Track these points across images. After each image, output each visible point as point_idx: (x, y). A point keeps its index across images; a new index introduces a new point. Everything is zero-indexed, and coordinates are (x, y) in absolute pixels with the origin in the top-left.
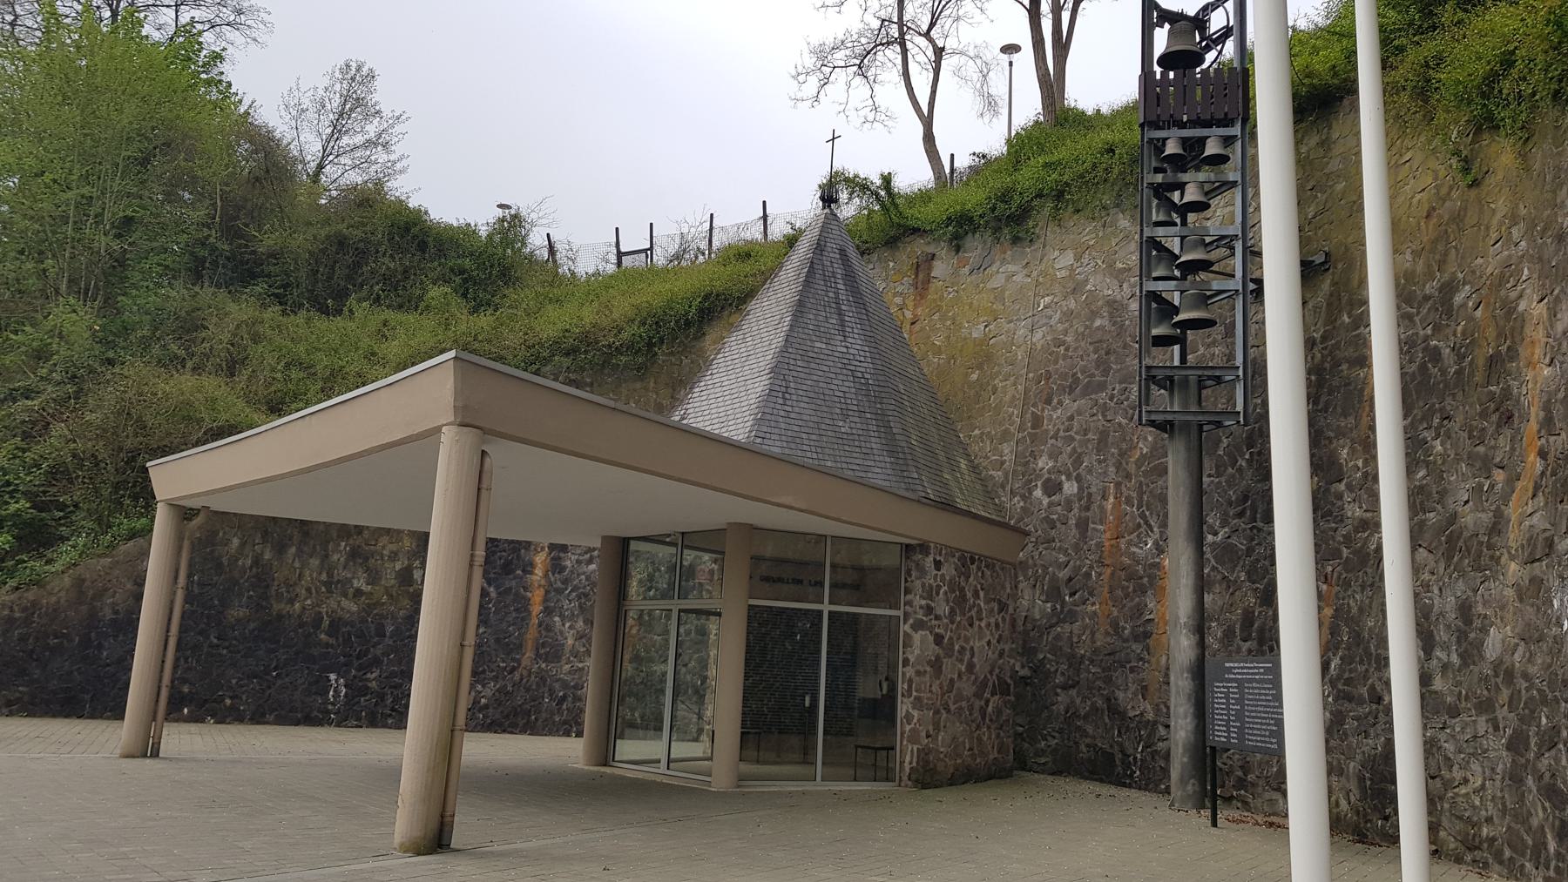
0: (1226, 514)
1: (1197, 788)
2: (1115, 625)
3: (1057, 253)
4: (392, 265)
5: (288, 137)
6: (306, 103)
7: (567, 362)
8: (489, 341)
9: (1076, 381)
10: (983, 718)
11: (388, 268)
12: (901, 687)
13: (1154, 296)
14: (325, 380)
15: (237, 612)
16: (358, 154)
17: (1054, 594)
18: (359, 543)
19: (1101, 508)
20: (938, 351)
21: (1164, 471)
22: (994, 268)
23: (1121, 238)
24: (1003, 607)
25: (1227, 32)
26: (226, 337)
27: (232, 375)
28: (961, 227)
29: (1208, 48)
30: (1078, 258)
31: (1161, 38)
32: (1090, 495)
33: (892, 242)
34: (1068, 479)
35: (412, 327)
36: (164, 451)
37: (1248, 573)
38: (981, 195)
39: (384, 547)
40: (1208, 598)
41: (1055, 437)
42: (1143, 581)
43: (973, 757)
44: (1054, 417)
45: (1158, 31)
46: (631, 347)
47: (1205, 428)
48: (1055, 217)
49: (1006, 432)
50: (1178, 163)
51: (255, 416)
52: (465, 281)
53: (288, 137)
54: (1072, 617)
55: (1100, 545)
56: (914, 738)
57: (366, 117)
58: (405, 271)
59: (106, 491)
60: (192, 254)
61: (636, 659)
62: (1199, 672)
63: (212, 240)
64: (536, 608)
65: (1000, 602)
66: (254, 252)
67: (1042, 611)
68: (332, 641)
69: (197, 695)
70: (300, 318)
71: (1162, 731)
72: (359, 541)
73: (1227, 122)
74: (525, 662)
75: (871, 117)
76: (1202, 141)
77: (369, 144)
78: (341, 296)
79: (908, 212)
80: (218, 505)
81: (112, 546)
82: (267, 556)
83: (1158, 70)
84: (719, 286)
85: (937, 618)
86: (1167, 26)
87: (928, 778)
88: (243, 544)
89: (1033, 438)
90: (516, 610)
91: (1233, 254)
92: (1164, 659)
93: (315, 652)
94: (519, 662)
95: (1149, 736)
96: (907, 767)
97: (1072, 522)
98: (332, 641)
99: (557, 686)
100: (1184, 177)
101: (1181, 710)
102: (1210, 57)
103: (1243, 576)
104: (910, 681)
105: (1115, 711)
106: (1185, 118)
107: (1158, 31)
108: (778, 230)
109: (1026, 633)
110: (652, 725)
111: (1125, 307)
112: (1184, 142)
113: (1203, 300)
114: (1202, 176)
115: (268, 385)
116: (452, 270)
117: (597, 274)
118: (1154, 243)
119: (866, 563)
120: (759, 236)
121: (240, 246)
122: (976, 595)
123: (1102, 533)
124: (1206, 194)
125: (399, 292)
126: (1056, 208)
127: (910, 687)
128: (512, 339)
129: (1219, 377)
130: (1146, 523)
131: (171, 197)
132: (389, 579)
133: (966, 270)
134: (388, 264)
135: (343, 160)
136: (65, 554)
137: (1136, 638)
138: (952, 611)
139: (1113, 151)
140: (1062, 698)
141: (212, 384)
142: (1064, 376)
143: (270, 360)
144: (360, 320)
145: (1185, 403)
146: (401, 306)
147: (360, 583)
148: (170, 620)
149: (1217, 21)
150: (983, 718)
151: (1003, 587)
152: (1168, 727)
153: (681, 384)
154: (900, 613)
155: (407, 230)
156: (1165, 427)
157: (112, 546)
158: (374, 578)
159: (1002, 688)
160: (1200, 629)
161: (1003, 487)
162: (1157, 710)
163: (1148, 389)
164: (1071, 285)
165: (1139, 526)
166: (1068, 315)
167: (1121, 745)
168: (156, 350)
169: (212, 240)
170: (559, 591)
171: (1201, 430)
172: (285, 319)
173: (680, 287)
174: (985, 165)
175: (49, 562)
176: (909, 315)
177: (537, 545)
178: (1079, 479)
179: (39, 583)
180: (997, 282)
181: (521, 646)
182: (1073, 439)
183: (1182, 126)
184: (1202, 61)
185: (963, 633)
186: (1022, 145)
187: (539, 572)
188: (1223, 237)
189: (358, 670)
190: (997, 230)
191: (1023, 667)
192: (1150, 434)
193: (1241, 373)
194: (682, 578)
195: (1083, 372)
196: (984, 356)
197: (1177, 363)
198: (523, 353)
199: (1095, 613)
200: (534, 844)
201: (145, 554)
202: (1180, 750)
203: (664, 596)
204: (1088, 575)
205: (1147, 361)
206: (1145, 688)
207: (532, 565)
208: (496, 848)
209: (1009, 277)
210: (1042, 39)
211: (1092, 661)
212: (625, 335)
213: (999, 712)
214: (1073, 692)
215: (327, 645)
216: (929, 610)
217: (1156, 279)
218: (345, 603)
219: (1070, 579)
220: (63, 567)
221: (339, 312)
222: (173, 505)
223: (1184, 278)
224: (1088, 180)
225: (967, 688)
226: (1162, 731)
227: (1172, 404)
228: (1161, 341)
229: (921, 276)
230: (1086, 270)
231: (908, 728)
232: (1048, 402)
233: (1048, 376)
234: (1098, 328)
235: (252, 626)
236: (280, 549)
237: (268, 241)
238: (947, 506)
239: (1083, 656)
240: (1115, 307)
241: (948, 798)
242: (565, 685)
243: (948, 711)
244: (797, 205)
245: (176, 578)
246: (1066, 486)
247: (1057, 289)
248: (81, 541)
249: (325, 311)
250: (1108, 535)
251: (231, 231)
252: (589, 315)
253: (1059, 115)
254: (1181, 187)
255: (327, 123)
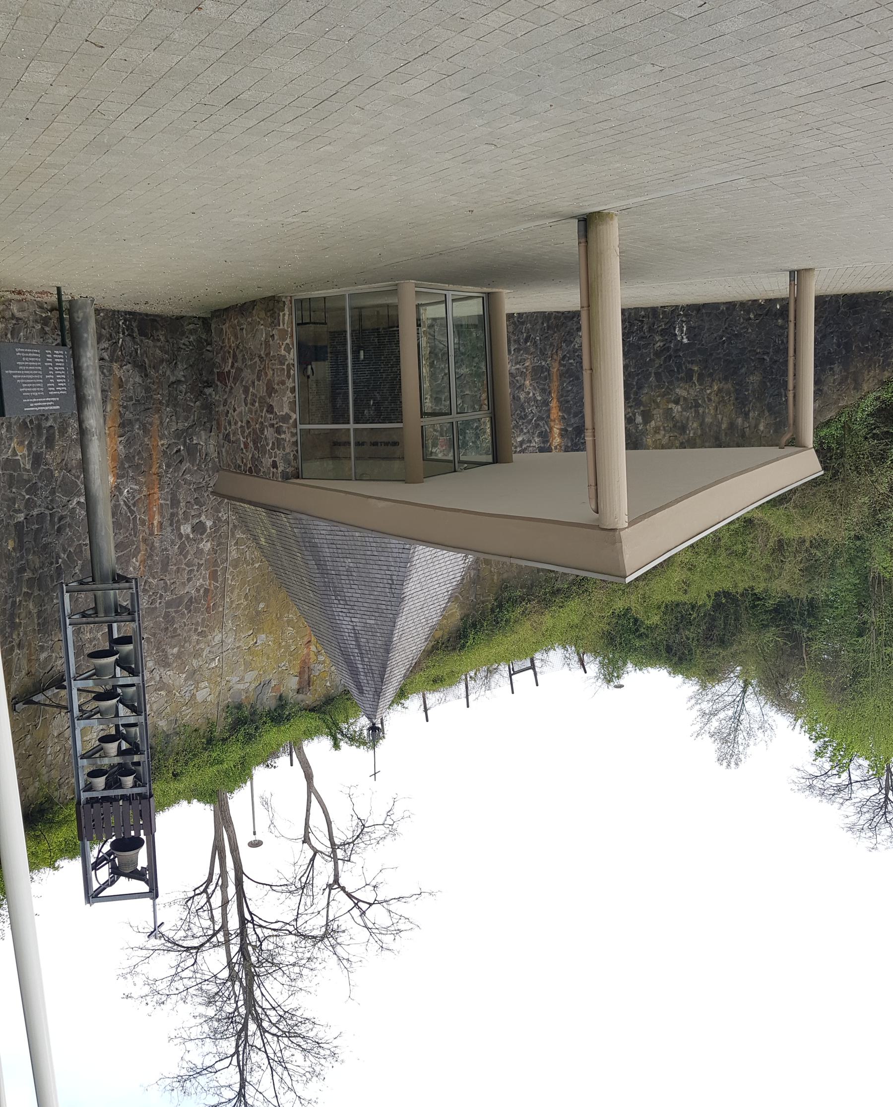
0: (72, 518)
1: (75, 315)
2: (146, 431)
3: (209, 699)
4: (687, 633)
5: (768, 706)
6: (759, 733)
7: (559, 585)
8: (614, 591)
9: (188, 608)
10: (234, 352)
11: (689, 630)
12: (294, 372)
13: (133, 673)
14: (719, 547)
15: (754, 379)
16: (721, 705)
17: (192, 450)
18: (683, 437)
19: (161, 514)
20: (289, 622)
21: (117, 546)
22: (253, 686)
23: (160, 712)
24: (227, 437)
25: (96, 866)
26: (787, 566)
27: (779, 541)
28: (280, 714)
29: (109, 854)
30: (193, 696)
31: (142, 861)
32: (171, 525)
33: (329, 700)
34: (188, 535)
35: (665, 591)
36: (815, 483)
37: (52, 476)
38: (266, 738)
39: (664, 436)
40: (79, 456)
41: (200, 565)
42: (127, 465)
43: (239, 324)
44: (201, 580)
45: (145, 865)
46: (514, 602)
47: (90, 579)
48: (212, 725)
49: (235, 566)
50: (124, 770)
51: (760, 515)
52: (637, 630)
53: (768, 706)
54: (178, 434)
55: (161, 489)
56: (283, 334)
57: (719, 732)
58: (677, 630)
59: (848, 451)
60: (816, 619)
61: (478, 375)
62: (81, 402)
63: (805, 630)
64: (554, 404)
65: (229, 441)
66: (778, 626)
67: (199, 437)
68: (689, 366)
69: (768, 319)
70: (741, 587)
71: (106, 356)
72: (682, 438)
73: (92, 801)
74: (556, 365)
75: (353, 790)
76: (108, 786)
77: (714, 714)
78: (717, 606)
79: (319, 723)
80: (774, 451)
81: (840, 414)
82: (740, 420)
83: (143, 836)
84: (455, 656)
85: (272, 425)
86: (139, 868)
87: (270, 305)
88: (756, 426)
89: (215, 564)
90: (568, 402)
91: (79, 706)
92: (108, 409)
93: (700, 357)
94: (560, 365)
95: (115, 351)
96: (287, 312)
97: (182, 504)
98: (689, 366)
99: (532, 350)
100: (117, 760)
101: (91, 372)
102: (107, 848)
103: (56, 474)
104: (289, 376)
105: (141, 367)
106: (121, 803)
107: (145, 865)
108: (414, 703)
109: (210, 420)
110: (461, 328)
111: (157, 663)
112: (120, 786)
113: (98, 673)
114: (106, 761)
115: (755, 537)
116: (647, 636)
117: (547, 651)
118: (136, 711)
119: (330, 462)
120: (428, 695)
121: (787, 629)
122: (246, 445)
123: (160, 497)
124: (102, 749)
125: (679, 615)
126: (211, 732)
127: (289, 372)
128: (598, 595)
129: (84, 617)
130: (129, 507)
131: (836, 654)
132: (657, 413)
133: (273, 683)
134: (690, 633)
135: (730, 699)
136: (869, 404)
137: (130, 422)
138: (262, 432)
139: (174, 775)
140: (180, 374)
141: (791, 533)
142: (197, 610)
143: (756, 555)
144: (701, 593)
145: (106, 597)
146: (677, 605)
147: (676, 409)
148: (795, 369)
149: (104, 874)
150: (234, 352)
151: (227, 452)
152: (102, 359)
153: (472, 582)
154: (300, 427)
155: (680, 659)
156: (118, 578)
157: (840, 414)
158: (668, 413)
159: (223, 377)
160: (82, 432)
161: (235, 526)
162: (110, 370)
163: (133, 605)
164: (197, 676)
165: (134, 505)
166: (197, 654)
167: (135, 343)
168: (830, 550)
169: (805, 630)
170: (541, 418)
171: (93, 580)
172: (751, 584)
173: (484, 652)
174: (267, 758)
175: (878, 398)
176: (313, 648)
177: (560, 450)
178: (180, 536)
179: (883, 383)
180: (250, 676)
181: (560, 376)
182: (187, 565)
183: (123, 797)
184: (112, 844)
185: (253, 416)
186: (241, 774)
187: (556, 431)
188: (88, 718)
189: (669, 348)
190: (253, 713)
191: (210, 395)
192: (131, 573)
193: (68, 621)
194: (457, 436)
195: (183, 614)
196: (256, 621)
197: (115, 625)
198: (590, 587)
199: (161, 439)
200: (522, 227)
201: (817, 412)
202: (89, 342)
203: (467, 423)
204: (168, 466)
205: (134, 625)
206: (120, 386)
207: (561, 436)
208: (547, 221)
209: (242, 679)
210: (232, 853)
211: (160, 402)
212: (519, 610)
213: (224, 359)
214: (173, 379)
215: (692, 362)
216: (278, 431)
217: (133, 685)
218: (685, 394)
219: (181, 462)
220: (868, 397)
221: (717, 595)
222: (804, 447)
223: (115, 687)
224: (190, 754)
225: (248, 375)
226: (106, 356)
227: (115, 594)
228: (126, 640)
229: (306, 677)
230: (183, 689)
231: (288, 341)
232: (207, 591)
233: (208, 610)
234: (175, 646)
235: (743, 370)
236: (732, 425)
237: (770, 635)
238: (272, 509)
239: (167, 406)
240: (164, 662)
241: (253, 292)
242: (527, 350)
243: (260, 356)
244: (401, 721)
245: (794, 397)
246: (189, 530)
247: (207, 673)
248: (860, 415)
249: (727, 594)
250: (156, 496)
251: (794, 637)
252: (548, 620)
253: (215, 797)
254: (121, 753)
255: (744, 722)
